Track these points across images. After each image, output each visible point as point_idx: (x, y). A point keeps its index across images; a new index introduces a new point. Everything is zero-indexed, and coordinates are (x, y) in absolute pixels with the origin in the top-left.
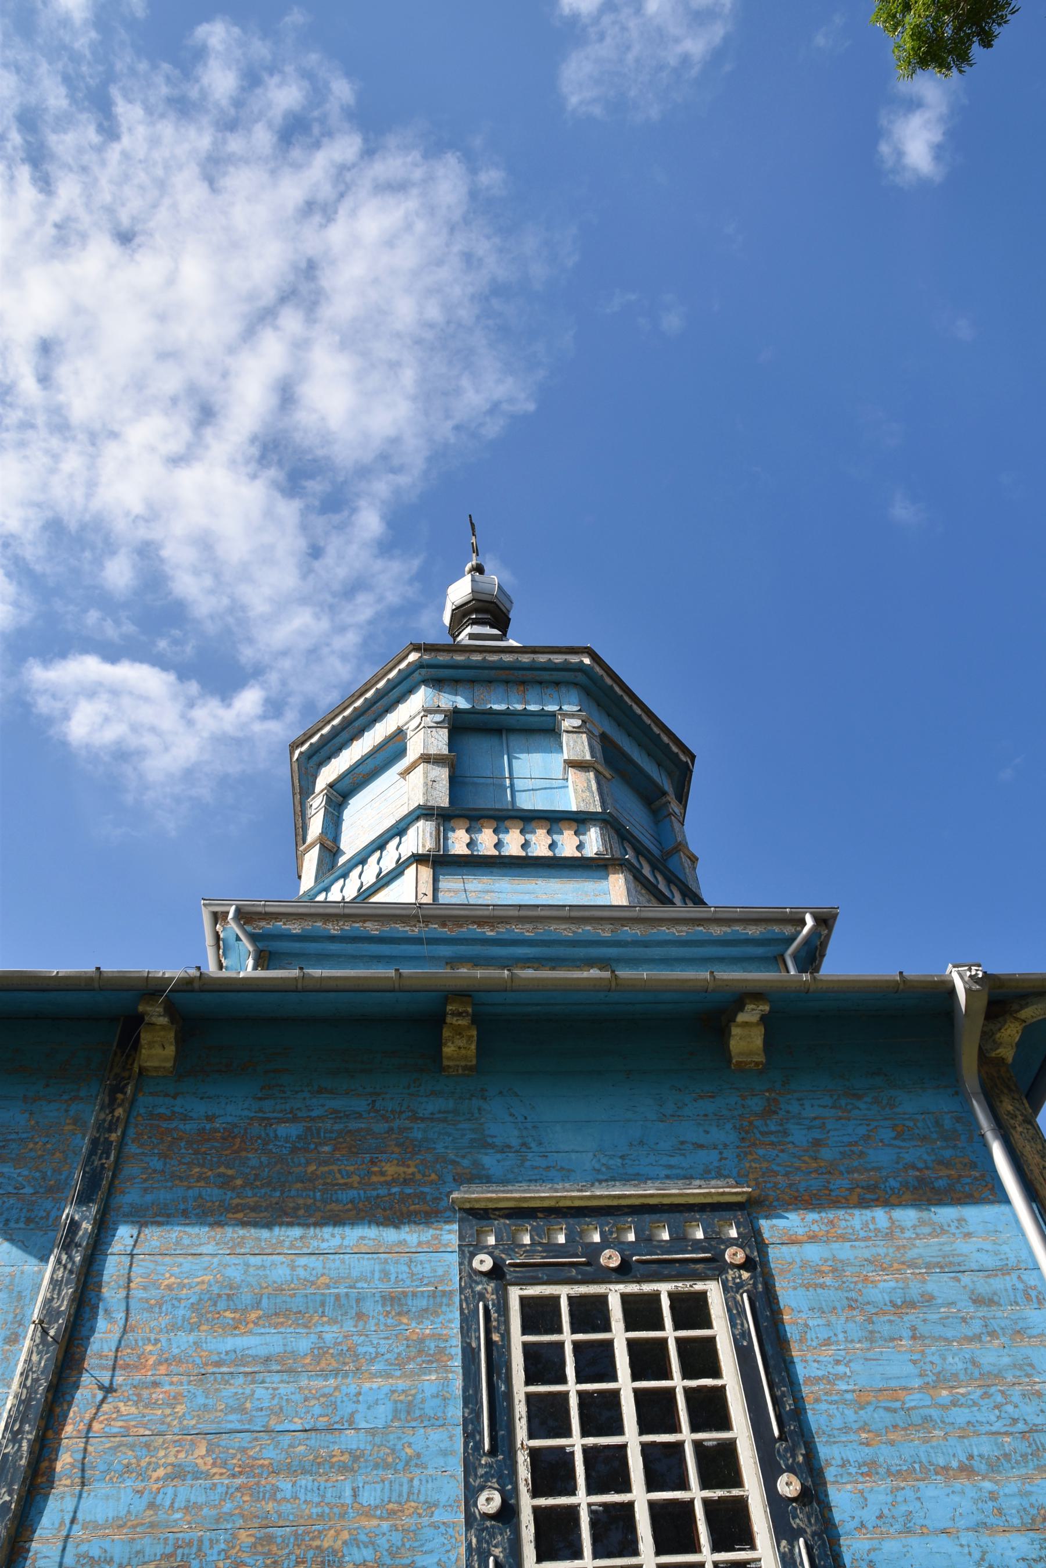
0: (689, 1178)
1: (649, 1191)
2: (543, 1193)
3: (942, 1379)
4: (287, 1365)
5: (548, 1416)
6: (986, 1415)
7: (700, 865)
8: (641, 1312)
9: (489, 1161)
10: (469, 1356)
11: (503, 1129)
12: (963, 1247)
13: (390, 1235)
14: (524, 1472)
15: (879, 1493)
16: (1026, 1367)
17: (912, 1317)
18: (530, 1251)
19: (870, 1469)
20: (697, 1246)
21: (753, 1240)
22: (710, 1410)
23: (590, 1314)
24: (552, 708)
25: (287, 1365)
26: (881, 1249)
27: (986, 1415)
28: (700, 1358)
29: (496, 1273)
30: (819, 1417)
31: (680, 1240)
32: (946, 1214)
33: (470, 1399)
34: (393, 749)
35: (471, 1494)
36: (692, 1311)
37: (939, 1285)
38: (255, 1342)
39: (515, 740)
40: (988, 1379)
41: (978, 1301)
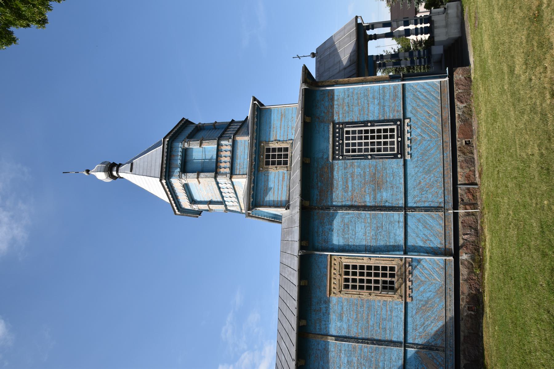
0: (329, 131)
1: (331, 136)
2: (331, 150)
3: (358, 104)
4: (353, 181)
5: (360, 150)
6: (362, 100)
7: (236, 120)
8: (348, 139)
9: (325, 157)
10: (353, 159)
11: (320, 155)
12: (341, 97)
13: (336, 169)
14: (366, 153)
15: (370, 114)
16: (357, 93)
17: (350, 106)
18: (339, 152)
19: (368, 115)
20: (339, 131)
21: (339, 123)
22: (360, 132)
23: (348, 145)
24: (180, 149)
25: (353, 181)
26: (341, 107)
27: (362, 100)
28: (354, 132)
29: (342, 156)
30: (362, 119)
31: (339, 133)
32: (336, 98)
33: (358, 159)
34: (186, 187)
35: (369, 159)
36: (348, 132)
37: (346, 101)
38: (350, 185)
39: (189, 158)
40: (358, 99)
41: (348, 97)
